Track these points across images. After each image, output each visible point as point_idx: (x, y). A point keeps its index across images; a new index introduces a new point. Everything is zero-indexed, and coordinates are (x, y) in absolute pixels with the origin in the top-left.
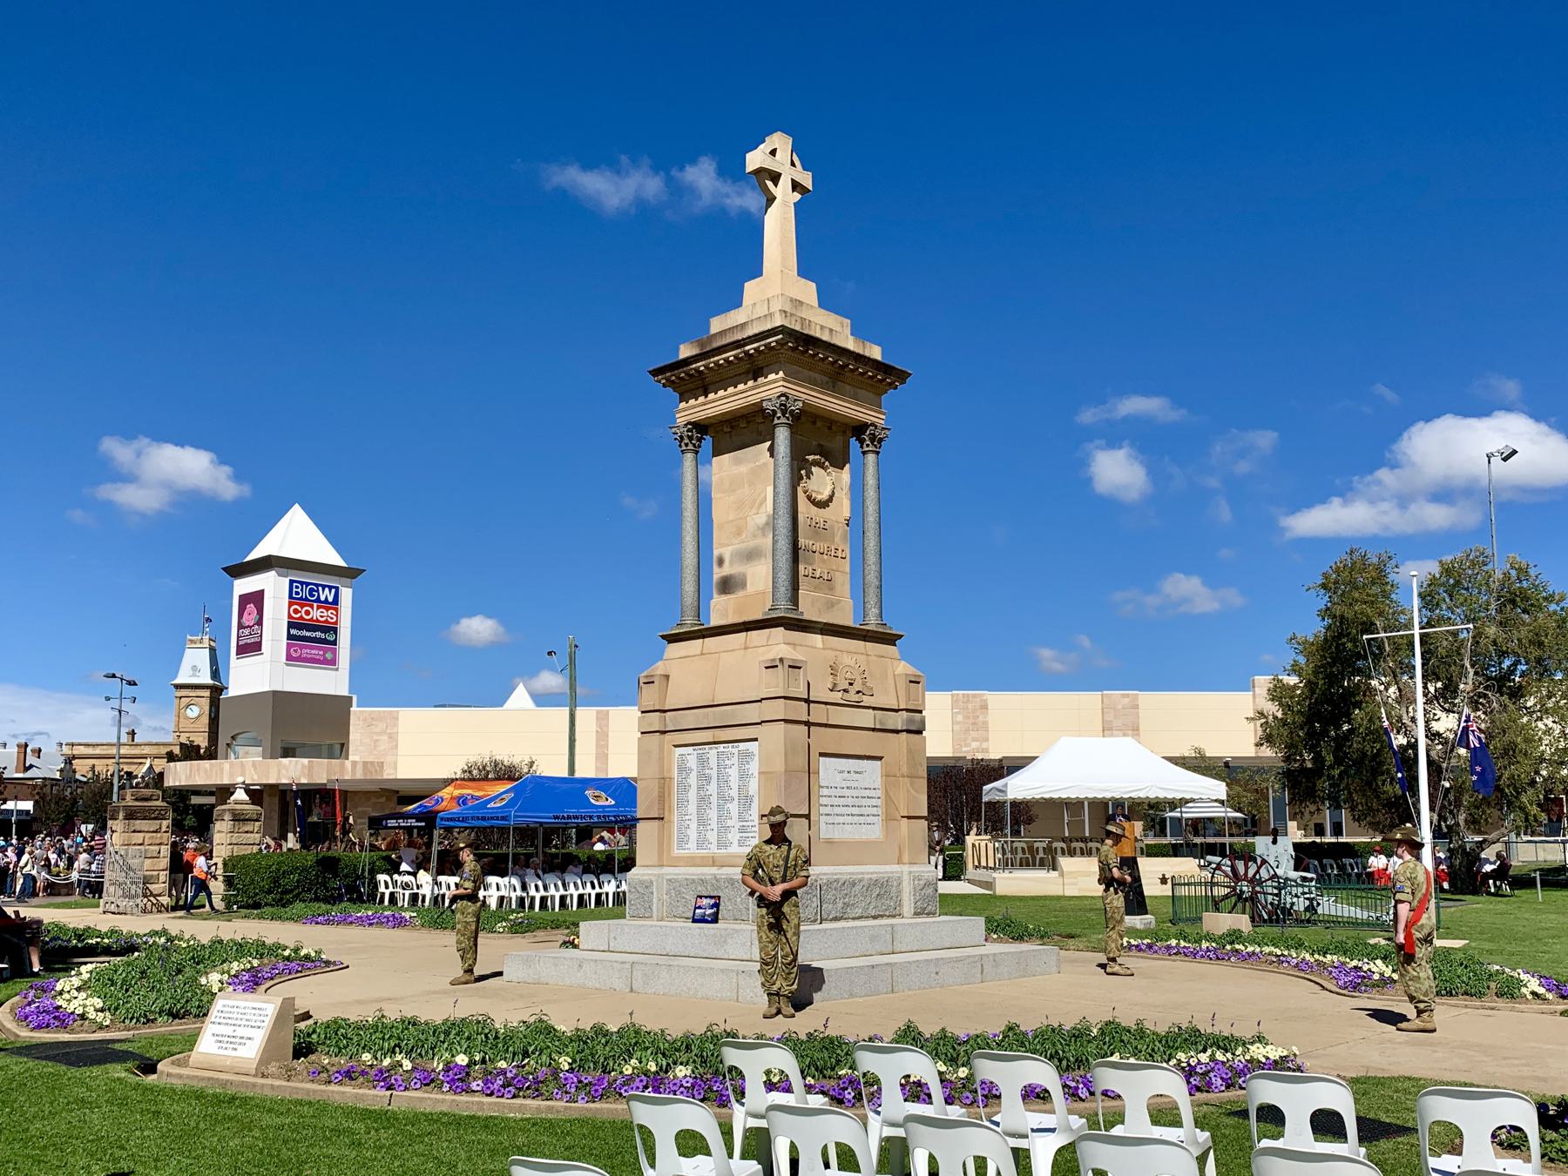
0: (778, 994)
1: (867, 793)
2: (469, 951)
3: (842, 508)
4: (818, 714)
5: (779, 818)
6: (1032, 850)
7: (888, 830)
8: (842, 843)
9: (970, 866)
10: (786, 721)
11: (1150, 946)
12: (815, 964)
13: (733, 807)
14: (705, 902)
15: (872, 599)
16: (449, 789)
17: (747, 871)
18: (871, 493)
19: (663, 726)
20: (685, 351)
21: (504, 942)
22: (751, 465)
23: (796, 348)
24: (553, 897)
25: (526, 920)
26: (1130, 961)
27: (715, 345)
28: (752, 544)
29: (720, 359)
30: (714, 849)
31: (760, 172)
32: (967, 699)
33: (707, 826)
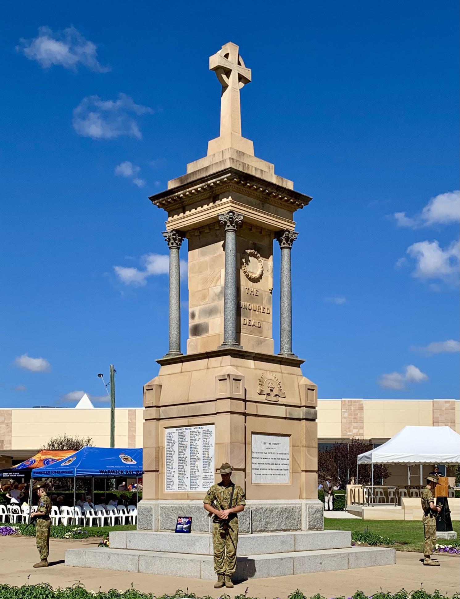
0: (224, 574)
1: (281, 456)
2: (44, 548)
3: (268, 283)
4: (251, 408)
5: (227, 471)
6: (387, 494)
7: (293, 479)
8: (265, 486)
9: (349, 502)
10: (231, 413)
11: (451, 549)
12: (250, 557)
13: (200, 464)
14: (183, 520)
15: (285, 339)
16: (39, 455)
17: (207, 501)
18: (286, 273)
19: (159, 415)
20: (171, 185)
21: (70, 544)
22: (212, 256)
23: (240, 182)
24: (100, 519)
25: (82, 532)
26: (440, 558)
27: (190, 180)
28: (212, 304)
29: (192, 189)
30: (188, 489)
31: (218, 68)
32: (351, 404)
33: (184, 476)
